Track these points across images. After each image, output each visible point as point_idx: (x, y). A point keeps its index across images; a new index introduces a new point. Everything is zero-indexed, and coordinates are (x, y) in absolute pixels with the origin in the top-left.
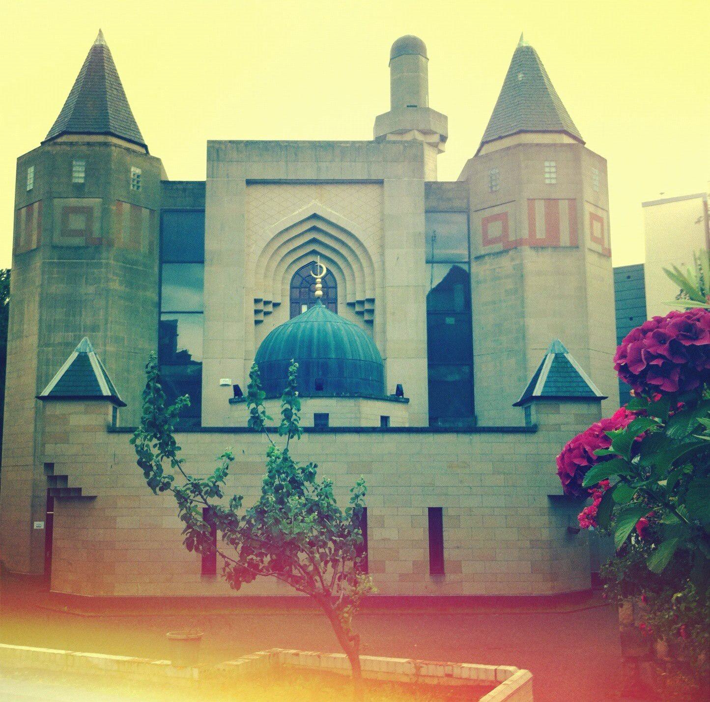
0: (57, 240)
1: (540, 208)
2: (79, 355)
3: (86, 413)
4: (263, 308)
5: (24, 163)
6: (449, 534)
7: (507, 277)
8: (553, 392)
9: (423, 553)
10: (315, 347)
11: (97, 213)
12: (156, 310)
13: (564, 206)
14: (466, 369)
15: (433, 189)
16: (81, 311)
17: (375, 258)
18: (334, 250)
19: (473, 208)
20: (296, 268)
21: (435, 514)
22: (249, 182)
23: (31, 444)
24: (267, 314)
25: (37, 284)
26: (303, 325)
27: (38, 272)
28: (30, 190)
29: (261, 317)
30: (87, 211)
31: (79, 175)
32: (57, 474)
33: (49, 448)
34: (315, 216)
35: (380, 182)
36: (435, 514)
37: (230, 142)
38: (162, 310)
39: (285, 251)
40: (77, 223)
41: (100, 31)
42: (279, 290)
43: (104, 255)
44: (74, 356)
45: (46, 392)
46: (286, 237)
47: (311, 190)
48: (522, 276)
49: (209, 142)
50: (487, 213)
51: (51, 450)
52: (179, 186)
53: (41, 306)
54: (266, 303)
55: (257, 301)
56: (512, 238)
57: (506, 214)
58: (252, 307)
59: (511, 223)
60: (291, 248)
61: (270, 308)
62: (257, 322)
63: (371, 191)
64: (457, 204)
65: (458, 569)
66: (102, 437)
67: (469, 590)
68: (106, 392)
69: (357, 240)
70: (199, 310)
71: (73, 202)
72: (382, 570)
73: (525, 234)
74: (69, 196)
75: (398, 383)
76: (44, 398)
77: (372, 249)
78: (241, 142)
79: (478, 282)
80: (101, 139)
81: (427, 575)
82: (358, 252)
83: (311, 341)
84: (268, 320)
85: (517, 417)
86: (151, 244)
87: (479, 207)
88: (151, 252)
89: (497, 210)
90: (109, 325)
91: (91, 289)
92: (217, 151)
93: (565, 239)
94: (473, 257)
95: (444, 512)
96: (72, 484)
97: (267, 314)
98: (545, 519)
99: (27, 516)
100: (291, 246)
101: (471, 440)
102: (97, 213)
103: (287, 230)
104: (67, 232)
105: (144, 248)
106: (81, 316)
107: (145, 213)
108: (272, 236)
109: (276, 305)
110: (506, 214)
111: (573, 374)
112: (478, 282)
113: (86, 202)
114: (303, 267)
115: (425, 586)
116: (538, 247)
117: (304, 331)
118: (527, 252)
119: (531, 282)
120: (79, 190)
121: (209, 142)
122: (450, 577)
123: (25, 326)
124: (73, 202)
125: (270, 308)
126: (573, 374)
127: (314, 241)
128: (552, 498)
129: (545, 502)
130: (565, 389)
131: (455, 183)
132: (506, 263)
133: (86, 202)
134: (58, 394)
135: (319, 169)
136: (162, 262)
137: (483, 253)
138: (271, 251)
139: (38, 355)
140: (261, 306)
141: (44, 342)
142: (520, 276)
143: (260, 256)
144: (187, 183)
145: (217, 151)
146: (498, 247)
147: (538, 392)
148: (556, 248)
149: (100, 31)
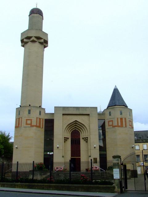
20: (71, 132)
34: (76, 121)
54: (85, 138)
55: (65, 138)
56: (114, 125)
61: (67, 139)
62: (65, 142)
63: (86, 117)
70: (65, 116)
92: (56, 108)
109: (68, 138)
125: (86, 139)
127: (76, 125)
138: (66, 129)
140: (65, 139)
145: (56, 108)
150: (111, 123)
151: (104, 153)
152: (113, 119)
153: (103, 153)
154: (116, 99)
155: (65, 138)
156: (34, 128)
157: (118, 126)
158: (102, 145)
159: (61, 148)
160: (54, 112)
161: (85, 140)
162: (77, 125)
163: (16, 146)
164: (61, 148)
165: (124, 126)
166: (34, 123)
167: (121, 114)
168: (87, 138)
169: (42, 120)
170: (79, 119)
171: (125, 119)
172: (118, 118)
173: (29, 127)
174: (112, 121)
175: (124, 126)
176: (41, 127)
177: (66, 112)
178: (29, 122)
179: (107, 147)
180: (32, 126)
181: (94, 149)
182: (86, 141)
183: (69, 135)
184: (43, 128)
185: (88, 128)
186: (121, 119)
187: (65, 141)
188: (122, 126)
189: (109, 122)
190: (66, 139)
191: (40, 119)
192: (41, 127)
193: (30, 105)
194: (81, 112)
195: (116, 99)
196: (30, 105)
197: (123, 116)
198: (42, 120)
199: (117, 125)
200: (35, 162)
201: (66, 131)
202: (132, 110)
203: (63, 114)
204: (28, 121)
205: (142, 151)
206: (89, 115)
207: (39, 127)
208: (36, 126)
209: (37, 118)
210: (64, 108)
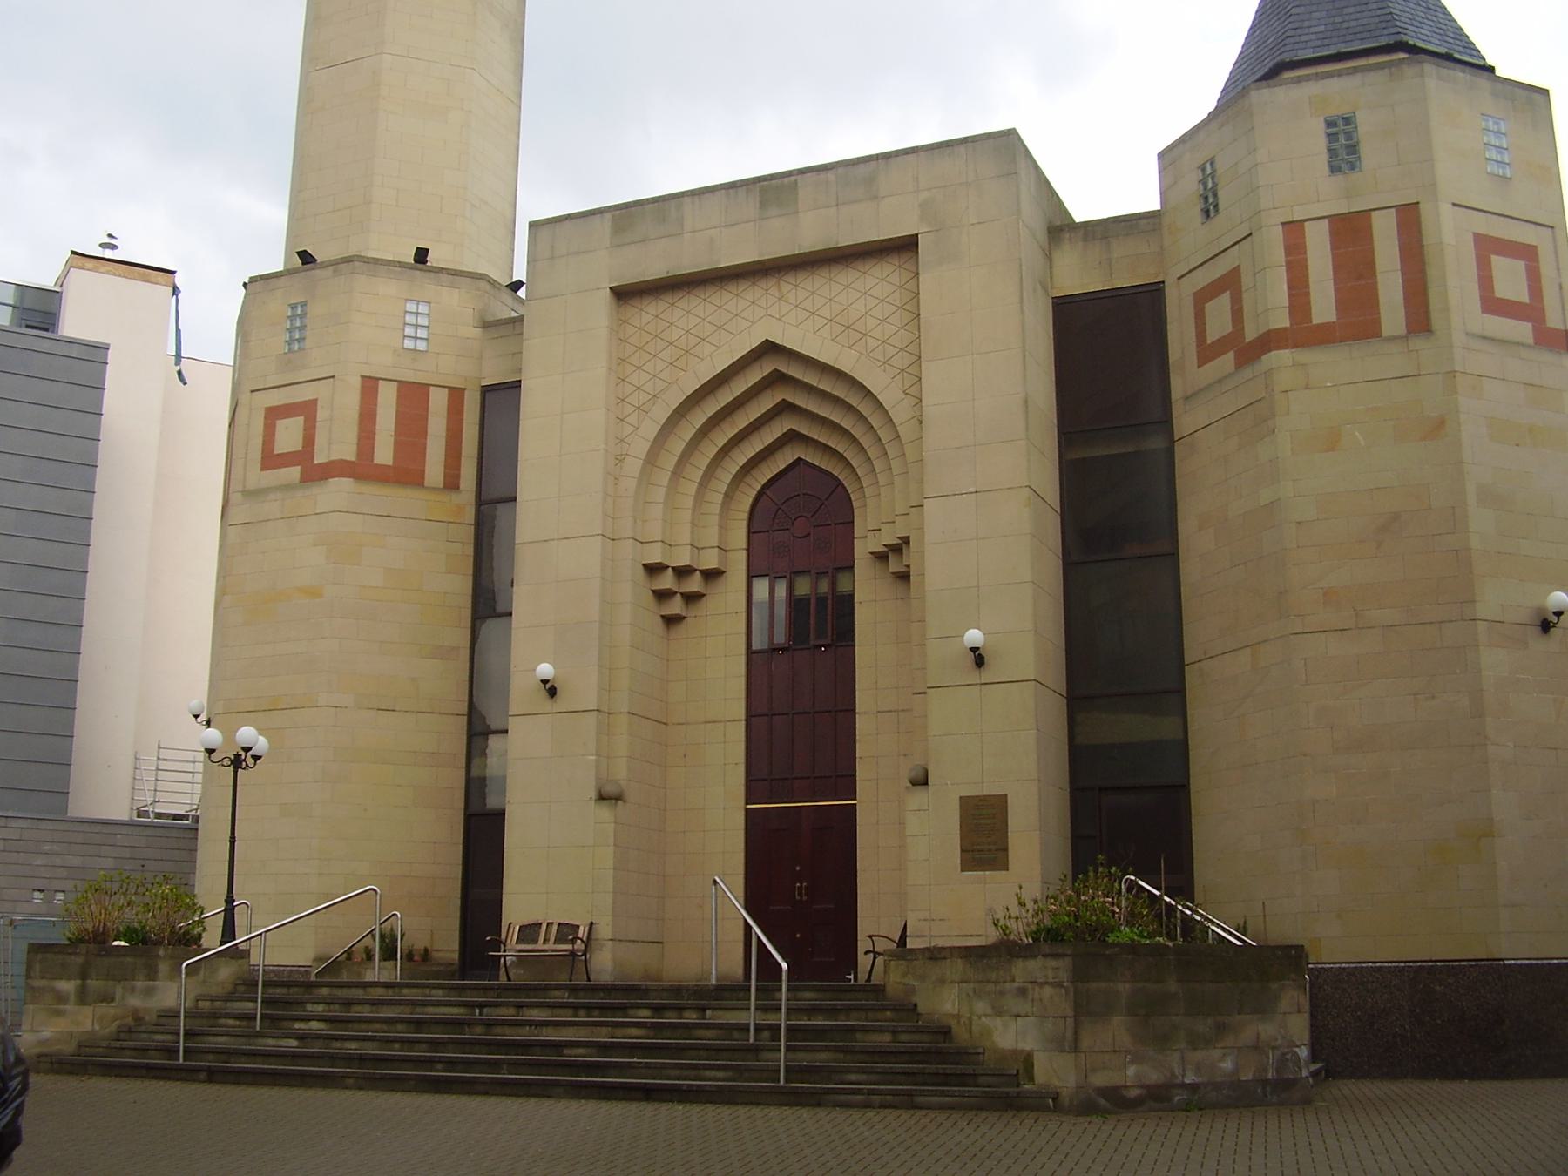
13: (1385, 233)
18: (826, 449)
24: (691, 598)
29: (676, 607)
32: (354, 448)
34: (769, 349)
46: (699, 417)
54: (682, 573)
55: (653, 570)
56: (1250, 334)
58: (645, 586)
62: (671, 621)
63: (880, 280)
70: (648, 312)
74: (232, 531)
75: (1355, 176)
97: (691, 598)
109: (711, 575)
125: (694, 584)
127: (785, 408)
138: (669, 461)
140: (667, 581)
150: (1219, 319)
151: (1166, 728)
153: (1124, 727)
156: (340, 489)
157: (1303, 334)
159: (583, 690)
161: (662, 596)
162: (800, 400)
163: (545, 670)
164: (583, 690)
165: (1392, 314)
166: (337, 443)
167: (1343, 145)
168: (671, 621)
169: (438, 402)
170: (802, 319)
171: (1409, 217)
172: (1294, 230)
173: (287, 487)
174: (307, 410)
175: (1392, 314)
176: (434, 469)
177: (657, 263)
178: (1510, 280)
179: (1189, 657)
180: (316, 474)
181: (974, 676)
182: (676, 607)
183: (714, 530)
184: (452, 484)
185: (901, 413)
186: (1350, 231)
188: (1358, 321)
189: (1203, 297)
190: (675, 592)
191: (413, 395)
192: (434, 469)
193: (421, 255)
194: (811, 230)
196: (421, 255)
197: (1378, 186)
198: (438, 402)
199: (1282, 320)
201: (677, 474)
202: (1012, 133)
203: (624, 294)
204: (282, 424)
206: (908, 245)
207: (406, 473)
208: (361, 469)
209: (370, 385)
210: (626, 217)
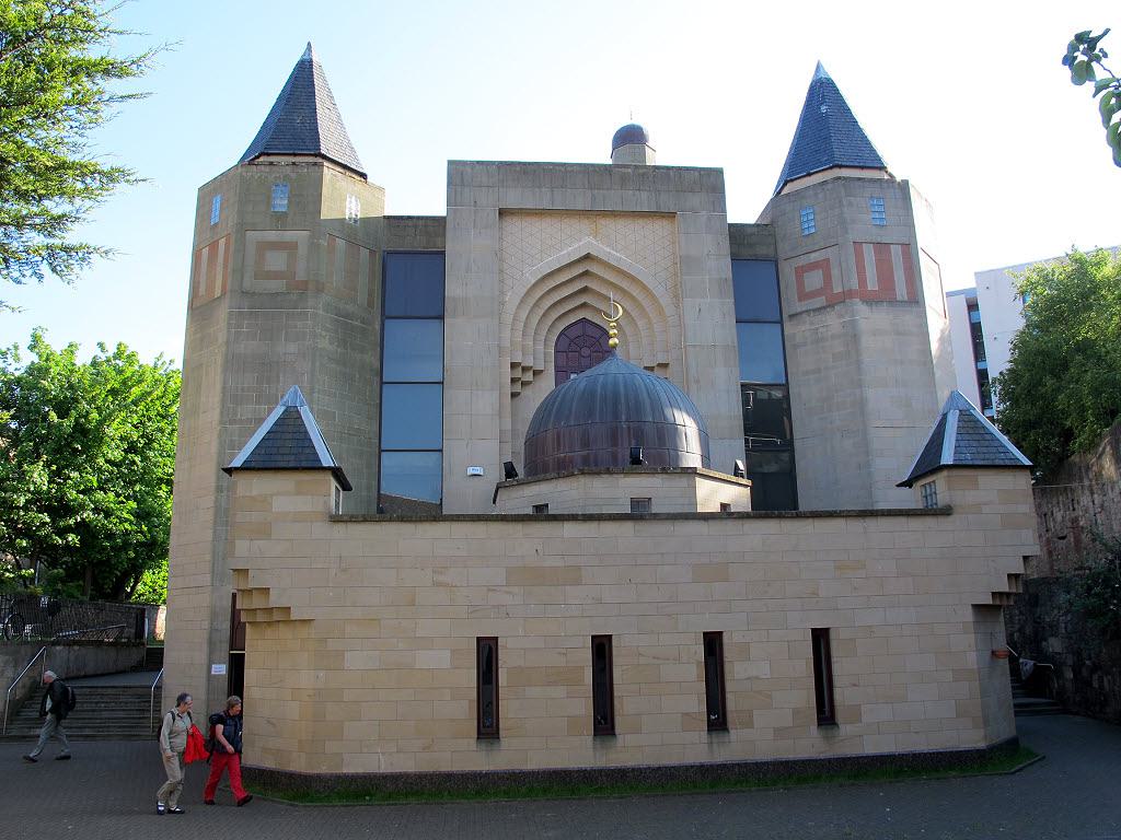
0: (248, 283)
1: (869, 254)
2: (286, 411)
3: (299, 493)
4: (522, 376)
5: (207, 193)
6: (841, 668)
7: (833, 337)
8: (968, 458)
9: (806, 697)
10: (623, 408)
11: (302, 250)
12: (377, 379)
14: (785, 456)
15: (737, 232)
16: (278, 377)
17: (669, 310)
19: (781, 255)
20: (561, 327)
21: (821, 638)
22: (502, 213)
23: (208, 557)
24: (524, 384)
25: (220, 341)
26: (601, 379)
27: (223, 324)
28: (216, 225)
29: (518, 388)
30: (291, 247)
31: (281, 203)
33: (242, 547)
34: (587, 257)
35: (672, 215)
36: (821, 638)
37: (478, 162)
38: (384, 380)
39: (548, 303)
40: (276, 261)
41: (309, 44)
42: (542, 355)
43: (311, 302)
44: (279, 411)
45: (237, 463)
47: (584, 225)
48: (855, 335)
49: (450, 162)
50: (803, 261)
51: (244, 550)
52: (410, 223)
53: (225, 370)
54: (525, 369)
55: (514, 366)
56: (837, 289)
57: (827, 260)
58: (507, 374)
59: (835, 272)
60: (541, 312)
61: (529, 376)
62: (514, 395)
64: (762, 251)
65: (856, 715)
66: (323, 530)
67: (872, 746)
68: (327, 460)
69: (644, 287)
71: (272, 236)
72: (749, 724)
73: (855, 284)
76: (229, 471)
77: (665, 301)
78: (492, 163)
79: (795, 347)
80: (311, 159)
81: (814, 727)
82: (645, 303)
83: (616, 395)
84: (527, 392)
85: (911, 498)
86: (370, 294)
87: (790, 254)
88: (370, 304)
89: (814, 257)
90: (316, 395)
91: (292, 348)
92: (461, 175)
93: (901, 291)
94: (785, 316)
95: (833, 635)
96: (275, 600)
97: (524, 384)
98: (972, 637)
99: (201, 656)
100: (557, 296)
101: (865, 528)
102: (302, 250)
103: (559, 270)
104: (263, 275)
105: (362, 298)
106: (278, 382)
107: (365, 253)
108: (533, 282)
109: (536, 373)
110: (827, 260)
111: (988, 437)
112: (795, 347)
113: (289, 236)
114: (568, 327)
115: (809, 744)
116: (871, 300)
117: (604, 386)
118: (861, 309)
119: (867, 342)
120: (280, 221)
121: (450, 162)
122: (845, 729)
123: (203, 399)
124: (272, 236)
125: (529, 376)
126: (988, 437)
128: (977, 608)
129: (969, 615)
130: (982, 456)
131: (753, 225)
132: (832, 322)
133: (289, 236)
134: (253, 465)
135: (594, 198)
136: (385, 317)
137: (799, 310)
138: (532, 301)
139: (220, 436)
140: (518, 373)
141: (228, 417)
142: (853, 337)
143: (518, 308)
144: (418, 218)
145: (461, 175)
146: (820, 301)
147: (947, 457)
148: (893, 302)
149: (309, 44)
152: (830, 253)
154: (827, 134)
155: (514, 366)
158: (551, 511)
160: (440, 209)
174: (824, 265)
187: (518, 388)
195: (827, 134)
200: (506, 662)
205: (234, 596)
